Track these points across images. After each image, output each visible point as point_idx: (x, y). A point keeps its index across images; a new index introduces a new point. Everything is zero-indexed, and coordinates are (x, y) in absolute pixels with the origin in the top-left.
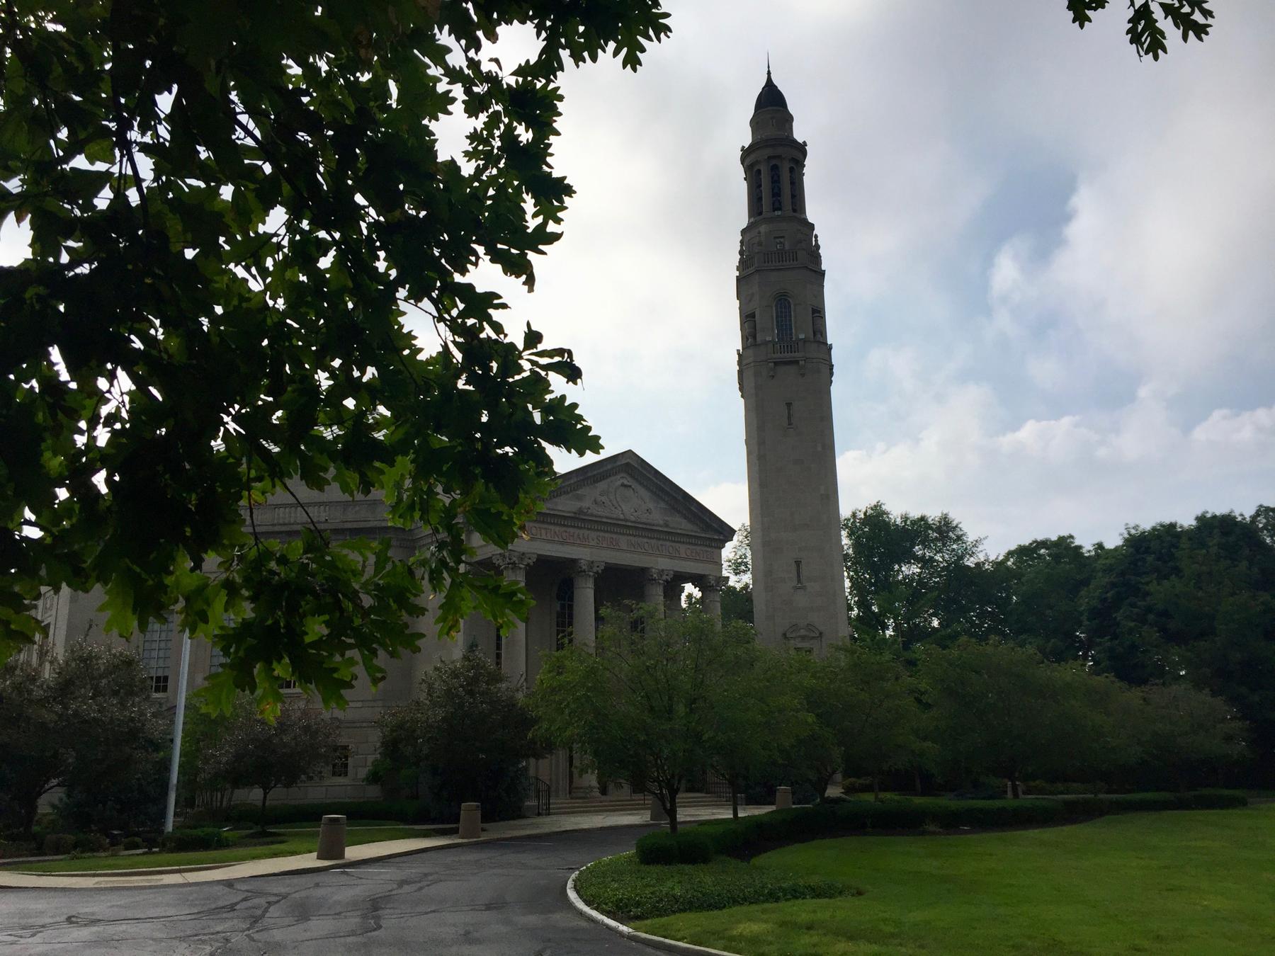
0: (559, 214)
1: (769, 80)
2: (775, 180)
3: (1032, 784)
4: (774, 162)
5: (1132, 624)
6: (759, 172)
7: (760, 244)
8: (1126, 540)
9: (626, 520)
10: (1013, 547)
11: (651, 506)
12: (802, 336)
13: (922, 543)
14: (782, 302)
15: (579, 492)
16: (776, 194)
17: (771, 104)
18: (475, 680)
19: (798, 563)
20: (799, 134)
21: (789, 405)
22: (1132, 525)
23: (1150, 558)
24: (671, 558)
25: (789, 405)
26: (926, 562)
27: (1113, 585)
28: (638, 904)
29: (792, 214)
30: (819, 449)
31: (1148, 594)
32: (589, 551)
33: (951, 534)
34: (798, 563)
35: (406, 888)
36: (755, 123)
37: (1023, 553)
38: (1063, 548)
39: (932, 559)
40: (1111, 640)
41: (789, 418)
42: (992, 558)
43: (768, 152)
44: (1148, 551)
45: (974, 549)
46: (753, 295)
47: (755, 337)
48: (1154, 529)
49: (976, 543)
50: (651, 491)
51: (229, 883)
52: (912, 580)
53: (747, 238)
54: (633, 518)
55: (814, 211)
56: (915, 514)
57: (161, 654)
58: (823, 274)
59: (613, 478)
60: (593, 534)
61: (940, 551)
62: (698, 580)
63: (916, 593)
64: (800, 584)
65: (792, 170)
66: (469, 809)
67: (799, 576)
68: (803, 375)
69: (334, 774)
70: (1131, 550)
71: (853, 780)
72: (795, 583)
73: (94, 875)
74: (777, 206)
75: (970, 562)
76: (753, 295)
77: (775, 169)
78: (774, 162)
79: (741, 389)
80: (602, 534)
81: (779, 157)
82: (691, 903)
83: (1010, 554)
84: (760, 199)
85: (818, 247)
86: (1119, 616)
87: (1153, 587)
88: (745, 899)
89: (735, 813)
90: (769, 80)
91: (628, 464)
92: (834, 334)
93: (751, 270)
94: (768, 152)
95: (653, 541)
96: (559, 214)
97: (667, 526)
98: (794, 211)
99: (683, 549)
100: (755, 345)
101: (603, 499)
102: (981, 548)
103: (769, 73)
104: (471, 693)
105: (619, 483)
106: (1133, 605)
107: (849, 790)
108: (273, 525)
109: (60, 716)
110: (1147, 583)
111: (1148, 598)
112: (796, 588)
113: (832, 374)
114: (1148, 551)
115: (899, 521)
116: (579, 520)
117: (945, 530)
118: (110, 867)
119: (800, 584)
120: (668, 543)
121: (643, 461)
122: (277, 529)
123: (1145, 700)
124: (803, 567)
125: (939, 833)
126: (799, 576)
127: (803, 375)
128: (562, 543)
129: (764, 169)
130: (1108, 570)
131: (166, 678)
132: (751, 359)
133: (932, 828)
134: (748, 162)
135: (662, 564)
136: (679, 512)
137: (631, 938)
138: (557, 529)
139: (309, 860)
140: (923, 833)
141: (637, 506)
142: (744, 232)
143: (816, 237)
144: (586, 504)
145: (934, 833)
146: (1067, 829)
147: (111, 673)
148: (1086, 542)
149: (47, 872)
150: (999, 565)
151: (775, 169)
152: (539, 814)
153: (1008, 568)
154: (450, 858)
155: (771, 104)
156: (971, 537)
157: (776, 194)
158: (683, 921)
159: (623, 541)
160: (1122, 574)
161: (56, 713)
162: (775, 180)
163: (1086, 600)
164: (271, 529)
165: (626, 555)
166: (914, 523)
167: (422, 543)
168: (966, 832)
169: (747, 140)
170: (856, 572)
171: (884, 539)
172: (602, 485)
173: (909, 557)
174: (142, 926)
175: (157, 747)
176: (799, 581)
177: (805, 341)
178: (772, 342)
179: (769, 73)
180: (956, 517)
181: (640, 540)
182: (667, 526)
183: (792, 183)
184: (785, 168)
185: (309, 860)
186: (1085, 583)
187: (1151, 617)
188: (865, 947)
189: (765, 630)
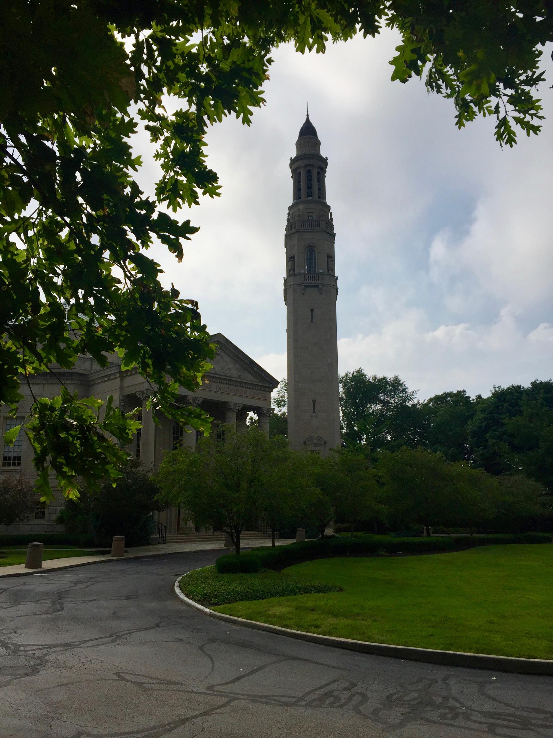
0: (218, 191)
4: (310, 168)
5: (494, 441)
6: (300, 173)
7: (299, 216)
10: (433, 396)
12: (321, 271)
14: (311, 250)
16: (309, 187)
17: (308, 133)
19: (314, 402)
20: (324, 153)
21: (312, 311)
22: (497, 386)
23: (506, 405)
26: (385, 403)
27: (486, 419)
29: (318, 199)
34: (314, 402)
36: (299, 144)
37: (438, 399)
40: (483, 449)
41: (312, 319)
43: (306, 162)
45: (412, 397)
47: (294, 270)
49: (413, 393)
55: (329, 200)
56: (380, 376)
58: (334, 236)
62: (256, 410)
63: (379, 421)
65: (319, 173)
67: (314, 410)
68: (321, 294)
74: (309, 194)
77: (309, 172)
78: (310, 168)
79: (285, 300)
81: (312, 165)
84: (300, 190)
85: (332, 220)
86: (488, 436)
87: (506, 421)
93: (293, 231)
94: (306, 162)
96: (218, 191)
97: (240, 378)
98: (319, 198)
99: (249, 391)
100: (294, 275)
102: (415, 396)
103: (308, 115)
113: (337, 294)
115: (371, 380)
117: (396, 386)
120: (239, 388)
121: (227, 340)
123: (499, 483)
126: (314, 410)
127: (321, 294)
129: (303, 171)
130: (484, 410)
132: (292, 283)
134: (293, 167)
135: (236, 399)
137: (211, 615)
139: (20, 569)
140: (379, 556)
142: (290, 208)
143: (331, 213)
145: (383, 556)
148: (472, 395)
151: (309, 172)
152: (159, 543)
155: (308, 133)
156: (410, 390)
157: (309, 187)
163: (470, 427)
166: (379, 381)
170: (346, 408)
171: (363, 389)
173: (376, 400)
176: (314, 412)
177: (322, 274)
178: (304, 273)
179: (308, 115)
180: (402, 378)
181: (224, 386)
182: (240, 378)
183: (319, 181)
185: (20, 569)
186: (471, 417)
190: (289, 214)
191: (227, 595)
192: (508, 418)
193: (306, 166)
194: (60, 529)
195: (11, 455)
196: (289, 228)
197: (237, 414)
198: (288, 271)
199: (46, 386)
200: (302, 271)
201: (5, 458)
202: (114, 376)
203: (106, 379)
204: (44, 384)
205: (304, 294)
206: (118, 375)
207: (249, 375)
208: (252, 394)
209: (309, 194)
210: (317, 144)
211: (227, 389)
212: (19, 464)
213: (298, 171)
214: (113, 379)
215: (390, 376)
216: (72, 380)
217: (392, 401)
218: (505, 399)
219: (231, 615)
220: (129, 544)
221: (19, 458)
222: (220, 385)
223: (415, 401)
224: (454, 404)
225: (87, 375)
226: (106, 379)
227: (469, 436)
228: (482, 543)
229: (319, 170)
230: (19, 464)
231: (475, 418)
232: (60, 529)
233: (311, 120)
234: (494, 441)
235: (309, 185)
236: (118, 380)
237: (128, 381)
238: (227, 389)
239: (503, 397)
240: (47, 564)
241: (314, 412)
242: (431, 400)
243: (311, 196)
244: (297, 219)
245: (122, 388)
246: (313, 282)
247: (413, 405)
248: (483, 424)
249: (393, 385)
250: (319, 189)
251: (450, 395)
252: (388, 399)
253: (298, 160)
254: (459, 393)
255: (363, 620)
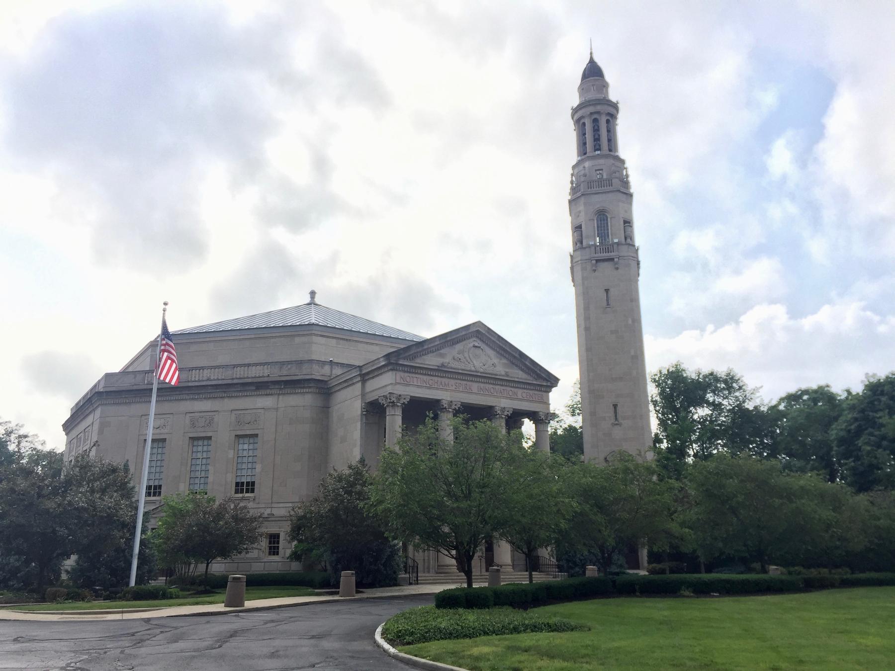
1: (591, 58)
2: (596, 130)
3: (792, 569)
4: (596, 116)
5: (869, 448)
6: (584, 124)
7: (585, 175)
8: (866, 386)
9: (476, 372)
10: (784, 395)
11: (496, 361)
12: (616, 241)
13: (713, 392)
14: (602, 216)
15: (442, 351)
16: (597, 139)
18: (352, 485)
19: (615, 406)
21: (607, 291)
22: (871, 374)
23: (884, 399)
24: (511, 399)
25: (607, 291)
26: (716, 407)
27: (856, 419)
28: (412, 634)
29: (608, 153)
30: (630, 322)
31: (882, 425)
32: (448, 394)
33: (734, 385)
34: (615, 406)
35: (269, 625)
36: (582, 89)
37: (792, 398)
38: (822, 395)
39: (720, 404)
40: (854, 461)
41: (607, 300)
42: (766, 402)
44: (882, 393)
45: (752, 396)
46: (580, 212)
47: (582, 243)
48: (887, 377)
49: (756, 390)
50: (498, 352)
51: (148, 620)
52: (706, 420)
53: (576, 171)
54: (482, 370)
55: (623, 151)
56: (706, 371)
57: (158, 470)
58: (631, 195)
59: (467, 341)
60: (452, 382)
61: (727, 398)
62: (533, 416)
63: (710, 432)
64: (616, 422)
65: (608, 121)
66: (348, 577)
67: (616, 416)
69: (270, 554)
70: (869, 393)
71: (654, 565)
72: (613, 421)
73: (62, 614)
74: (597, 147)
75: (749, 406)
76: (580, 212)
77: (595, 121)
78: (596, 116)
79: (573, 280)
80: (459, 381)
81: (598, 113)
82: (451, 634)
83: (782, 400)
84: (585, 144)
85: (627, 176)
86: (860, 442)
87: (885, 420)
88: (494, 632)
89: (531, 580)
90: (591, 58)
91: (478, 331)
92: (639, 239)
93: (579, 194)
95: (497, 387)
97: (508, 376)
98: (610, 150)
99: (520, 392)
100: (582, 248)
101: (460, 356)
102: (758, 394)
104: (349, 493)
105: (472, 345)
106: (871, 434)
107: (651, 572)
108: (233, 379)
109: (59, 505)
110: (880, 418)
111: (883, 429)
112: (614, 425)
113: (639, 268)
114: (882, 393)
116: (441, 371)
117: (730, 383)
118: (78, 608)
119: (616, 422)
121: (489, 329)
122: (235, 381)
123: (871, 502)
124: (619, 408)
125: (691, 597)
126: (616, 416)
127: (617, 269)
128: (429, 388)
130: (852, 408)
131: (160, 487)
132: (579, 259)
133: (687, 593)
134: (576, 117)
135: (504, 402)
136: (517, 366)
137: (395, 657)
138: (425, 377)
139: (220, 607)
141: (487, 361)
142: (574, 167)
144: (447, 360)
145: (688, 597)
146: (803, 595)
147: (103, 477)
148: (838, 388)
149: (31, 611)
150: (773, 408)
151: (595, 121)
152: (411, 584)
153: (778, 410)
154: (335, 608)
157: (597, 139)
158: (435, 646)
159: (475, 386)
160: (863, 411)
161: (56, 502)
162: (596, 130)
163: (835, 432)
164: (230, 382)
165: (477, 397)
166: (705, 377)
167: (334, 390)
168: (714, 596)
169: (576, 101)
170: (663, 414)
171: (682, 391)
172: (459, 347)
173: (701, 401)
174: (62, 643)
175: (124, 525)
176: (616, 419)
177: (618, 244)
180: (738, 372)
181: (487, 386)
182: (508, 376)
183: (609, 131)
184: (603, 120)
185: (220, 607)
186: (836, 419)
187: (885, 443)
188: (558, 664)
189: (594, 454)
190: (572, 175)
191: (426, 633)
192: (887, 417)
193: (591, 114)
194: (296, 567)
195: (244, 480)
196: (574, 190)
197: (507, 421)
198: (575, 244)
199: (281, 397)
200: (592, 243)
201: (237, 484)
202: (355, 381)
203: (346, 384)
204: (279, 394)
205: (595, 271)
206: (359, 379)
207: (521, 372)
208: (524, 395)
209: (597, 147)
210: (605, 86)
211: (492, 390)
212: (253, 491)
213: (582, 121)
214: (353, 384)
215: (721, 370)
216: (310, 387)
217: (725, 402)
218: (882, 391)
219: (416, 656)
220: (361, 585)
221: (253, 483)
222: (482, 385)
223: (757, 402)
224: (817, 406)
225: (326, 381)
226: (346, 384)
227: (834, 444)
228: (846, 584)
229: (608, 118)
230: (253, 491)
231: (842, 419)
232: (296, 567)
233: (596, 59)
234: (869, 448)
235: (597, 136)
236: (360, 384)
237: (372, 385)
238: (492, 390)
239: (880, 389)
240: (248, 604)
241: (616, 419)
242: (782, 400)
243: (599, 149)
244: (583, 179)
245: (363, 395)
246: (607, 254)
247: (756, 407)
248: (853, 427)
249: (725, 382)
250: (609, 140)
251: (806, 392)
252: (720, 400)
253: (581, 109)
254: (821, 388)
255: (587, 663)
